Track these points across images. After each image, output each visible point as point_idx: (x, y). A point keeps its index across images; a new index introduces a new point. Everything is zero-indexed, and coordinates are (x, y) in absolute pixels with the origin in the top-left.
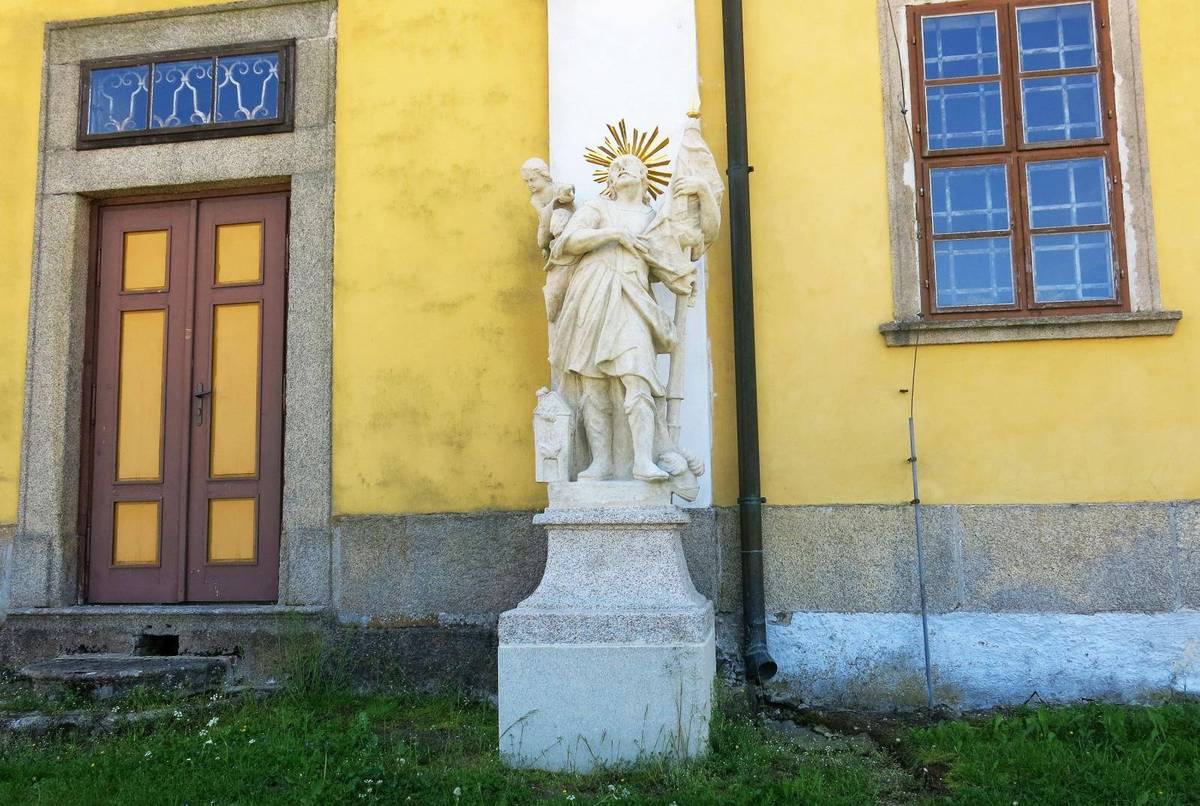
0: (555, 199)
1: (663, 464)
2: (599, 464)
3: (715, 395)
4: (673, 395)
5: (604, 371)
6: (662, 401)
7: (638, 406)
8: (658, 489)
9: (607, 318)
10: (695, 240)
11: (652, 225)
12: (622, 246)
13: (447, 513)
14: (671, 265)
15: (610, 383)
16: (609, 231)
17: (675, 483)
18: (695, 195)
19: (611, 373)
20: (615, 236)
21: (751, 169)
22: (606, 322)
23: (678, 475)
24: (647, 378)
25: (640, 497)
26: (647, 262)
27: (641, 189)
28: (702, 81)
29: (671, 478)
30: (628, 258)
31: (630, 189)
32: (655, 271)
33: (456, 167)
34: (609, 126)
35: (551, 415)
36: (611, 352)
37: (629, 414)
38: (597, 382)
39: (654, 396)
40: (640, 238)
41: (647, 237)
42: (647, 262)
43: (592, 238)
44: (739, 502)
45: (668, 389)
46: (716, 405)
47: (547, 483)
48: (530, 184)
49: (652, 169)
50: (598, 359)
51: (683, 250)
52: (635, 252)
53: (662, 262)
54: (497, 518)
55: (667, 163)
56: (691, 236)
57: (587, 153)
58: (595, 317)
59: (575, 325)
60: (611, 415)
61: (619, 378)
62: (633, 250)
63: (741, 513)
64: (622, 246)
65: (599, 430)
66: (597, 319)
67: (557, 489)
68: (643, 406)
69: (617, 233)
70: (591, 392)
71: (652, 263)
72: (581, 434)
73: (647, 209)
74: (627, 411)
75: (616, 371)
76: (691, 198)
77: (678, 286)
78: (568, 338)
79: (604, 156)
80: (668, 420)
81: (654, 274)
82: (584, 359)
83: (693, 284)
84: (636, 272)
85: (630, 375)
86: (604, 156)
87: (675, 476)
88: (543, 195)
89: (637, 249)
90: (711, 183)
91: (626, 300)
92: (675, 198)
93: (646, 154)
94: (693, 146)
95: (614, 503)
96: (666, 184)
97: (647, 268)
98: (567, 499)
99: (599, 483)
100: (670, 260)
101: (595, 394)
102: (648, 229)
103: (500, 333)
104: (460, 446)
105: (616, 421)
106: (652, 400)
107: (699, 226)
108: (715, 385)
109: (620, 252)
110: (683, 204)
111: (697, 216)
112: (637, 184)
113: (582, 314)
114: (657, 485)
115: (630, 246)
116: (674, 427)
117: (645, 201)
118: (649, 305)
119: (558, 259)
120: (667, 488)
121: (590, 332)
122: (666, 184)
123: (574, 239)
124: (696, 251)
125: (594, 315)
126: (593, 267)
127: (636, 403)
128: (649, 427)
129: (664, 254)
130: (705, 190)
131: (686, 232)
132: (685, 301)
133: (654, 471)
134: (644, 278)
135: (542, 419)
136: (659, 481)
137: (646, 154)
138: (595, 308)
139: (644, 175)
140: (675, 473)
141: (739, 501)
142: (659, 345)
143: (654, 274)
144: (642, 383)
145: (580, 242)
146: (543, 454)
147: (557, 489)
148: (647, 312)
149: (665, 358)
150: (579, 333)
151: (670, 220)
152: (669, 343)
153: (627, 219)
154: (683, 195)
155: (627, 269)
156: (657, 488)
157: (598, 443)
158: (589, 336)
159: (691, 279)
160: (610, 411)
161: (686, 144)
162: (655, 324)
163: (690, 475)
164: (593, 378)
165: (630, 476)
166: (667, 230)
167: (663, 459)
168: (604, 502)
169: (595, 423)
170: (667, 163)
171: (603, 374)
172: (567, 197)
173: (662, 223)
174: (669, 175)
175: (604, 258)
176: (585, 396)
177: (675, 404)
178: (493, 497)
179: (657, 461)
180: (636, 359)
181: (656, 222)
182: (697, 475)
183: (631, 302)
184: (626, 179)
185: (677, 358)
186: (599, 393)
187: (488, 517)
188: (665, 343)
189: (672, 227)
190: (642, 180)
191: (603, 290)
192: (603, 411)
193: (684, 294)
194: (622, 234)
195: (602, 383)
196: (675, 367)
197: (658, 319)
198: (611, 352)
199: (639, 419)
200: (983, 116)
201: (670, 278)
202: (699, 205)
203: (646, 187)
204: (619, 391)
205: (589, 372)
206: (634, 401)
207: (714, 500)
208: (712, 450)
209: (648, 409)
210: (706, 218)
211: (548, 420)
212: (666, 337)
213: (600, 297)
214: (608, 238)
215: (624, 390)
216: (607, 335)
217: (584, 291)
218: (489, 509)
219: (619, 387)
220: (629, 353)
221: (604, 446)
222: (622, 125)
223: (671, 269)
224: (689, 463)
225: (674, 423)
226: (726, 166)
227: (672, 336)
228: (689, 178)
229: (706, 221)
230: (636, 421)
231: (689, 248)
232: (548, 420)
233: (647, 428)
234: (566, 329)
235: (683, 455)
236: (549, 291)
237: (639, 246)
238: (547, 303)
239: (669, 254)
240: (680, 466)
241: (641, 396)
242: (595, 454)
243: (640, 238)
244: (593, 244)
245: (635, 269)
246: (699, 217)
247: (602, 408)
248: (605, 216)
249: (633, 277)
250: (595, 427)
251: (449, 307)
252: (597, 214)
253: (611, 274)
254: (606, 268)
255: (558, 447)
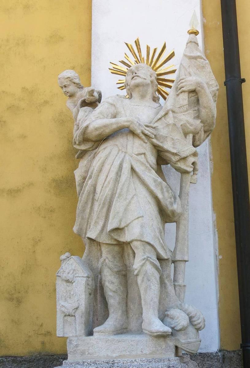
0: (83, 99)
1: (169, 320)
2: (110, 323)
3: (221, 257)
4: (178, 257)
5: (116, 237)
6: (167, 263)
7: (144, 268)
8: (163, 343)
9: (118, 191)
10: (195, 129)
11: (159, 116)
12: (133, 133)
13: (6, 357)
14: (174, 148)
15: (122, 249)
16: (122, 120)
17: (178, 337)
18: (194, 91)
19: (122, 239)
20: (126, 124)
21: (244, 81)
22: (117, 195)
23: (180, 330)
24: (152, 243)
25: (147, 351)
26: (155, 146)
27: (150, 90)
28: (205, 21)
29: (174, 332)
30: (137, 142)
31: (141, 88)
32: (162, 154)
33: (24, 89)
34: (127, 44)
35: (70, 277)
36: (121, 221)
37: (137, 275)
38: (111, 247)
39: (160, 259)
40: (147, 126)
41: (154, 126)
42: (155, 146)
43: (106, 126)
44: (241, 347)
45: (174, 253)
46: (221, 266)
47: (67, 338)
48: (64, 89)
49: (155, 68)
50: (110, 227)
51: (186, 137)
52: (143, 137)
53: (167, 146)
54: (45, 360)
55: (174, 71)
56: (191, 125)
57: (112, 66)
58: (107, 191)
59: (93, 199)
60: (125, 276)
61: (128, 243)
62: (141, 135)
63: (244, 355)
64: (133, 133)
65: (114, 290)
66: (110, 193)
67: (75, 343)
68: (149, 268)
69: (127, 121)
70: (107, 258)
71: (159, 146)
72: (98, 292)
73: (156, 105)
74: (136, 273)
75: (126, 237)
76: (191, 95)
77: (181, 165)
78: (88, 210)
79: (124, 68)
80: (175, 280)
81: (162, 159)
82: (99, 227)
83: (194, 164)
84: (144, 154)
85: (137, 240)
86: (124, 68)
87: (177, 331)
88: (76, 99)
89: (146, 135)
90: (207, 84)
91: (134, 175)
92: (178, 95)
93: (158, 65)
94: (192, 55)
95: (124, 356)
96: (170, 87)
97: (154, 151)
98: (83, 353)
99: (112, 337)
100: (173, 144)
101: (110, 257)
102: (156, 119)
103: (52, 211)
104: (19, 301)
105: (129, 281)
106: (157, 263)
107: (198, 117)
108: (220, 249)
109: (130, 138)
110: (184, 99)
111: (196, 108)
112: (147, 85)
113: (98, 189)
114: (162, 339)
115: (139, 131)
116: (180, 286)
117: (155, 99)
118: (155, 181)
119: (79, 144)
120: (171, 343)
121: (104, 204)
122: (170, 87)
123: (91, 127)
124: (197, 137)
125: (108, 189)
126: (106, 152)
127: (142, 266)
128: (155, 287)
129: (168, 139)
130: (202, 88)
131: (187, 121)
132: (188, 178)
133: (158, 326)
134: (152, 159)
135: (63, 280)
136: (163, 336)
137: (158, 65)
138: (109, 182)
139: (153, 78)
140: (178, 328)
141: (242, 346)
142: (165, 215)
143: (162, 159)
144: (148, 247)
145: (96, 129)
146: (63, 312)
147: (75, 343)
148: (152, 187)
149: (171, 227)
150: (96, 208)
151: (173, 112)
152: (173, 212)
153: (141, 113)
154: (184, 91)
155: (131, 153)
156: (161, 342)
157: (114, 301)
158: (103, 207)
159: (192, 159)
160: (124, 273)
161: (189, 54)
162: (160, 196)
163: (191, 330)
164: (107, 244)
165: (140, 331)
166: (170, 119)
167: (168, 315)
168: (114, 355)
169: (111, 282)
170: (174, 71)
171: (116, 240)
172: (91, 98)
173: (166, 114)
174: (172, 81)
175: (117, 143)
176: (102, 260)
177: (181, 265)
178: (43, 343)
179: (163, 317)
180: (142, 226)
181: (162, 113)
182: (198, 330)
183: (139, 177)
184: (138, 80)
185: (182, 227)
186: (114, 257)
187: (38, 360)
188: (169, 212)
189: (174, 117)
190: (152, 82)
191: (114, 169)
192: (118, 272)
193: (187, 172)
194: (132, 122)
195: (116, 248)
196: (181, 233)
197: (163, 193)
198: (121, 221)
199: (145, 278)
200: (247, 348)
201: (174, 159)
202: (198, 100)
203: (155, 88)
204: (131, 255)
205: (104, 239)
206: (141, 264)
207: (221, 346)
208: (220, 302)
209: (154, 270)
210: (203, 111)
211: (68, 281)
212: (170, 208)
213: (112, 175)
214: (120, 125)
215: (134, 253)
216: (118, 206)
217: (100, 171)
218: (40, 353)
219: (131, 252)
220: (136, 221)
221: (119, 303)
222: (137, 43)
223: (175, 151)
224: (191, 318)
225: (180, 282)
226: (224, 80)
227: (176, 207)
228: (190, 78)
229: (204, 112)
230: (143, 281)
231: (191, 136)
232: (68, 281)
233: (153, 287)
234: (86, 203)
235: (185, 311)
236: (78, 174)
237: (146, 132)
238: (77, 184)
239: (173, 139)
240: (181, 320)
241: (147, 259)
242: (111, 310)
243: (147, 126)
244: (108, 131)
245: (143, 151)
246: (199, 110)
247: (116, 270)
248: (121, 110)
249: (142, 158)
250: (110, 287)
251: (14, 193)
252: (113, 108)
253: (123, 155)
254: (119, 150)
255: (76, 305)
